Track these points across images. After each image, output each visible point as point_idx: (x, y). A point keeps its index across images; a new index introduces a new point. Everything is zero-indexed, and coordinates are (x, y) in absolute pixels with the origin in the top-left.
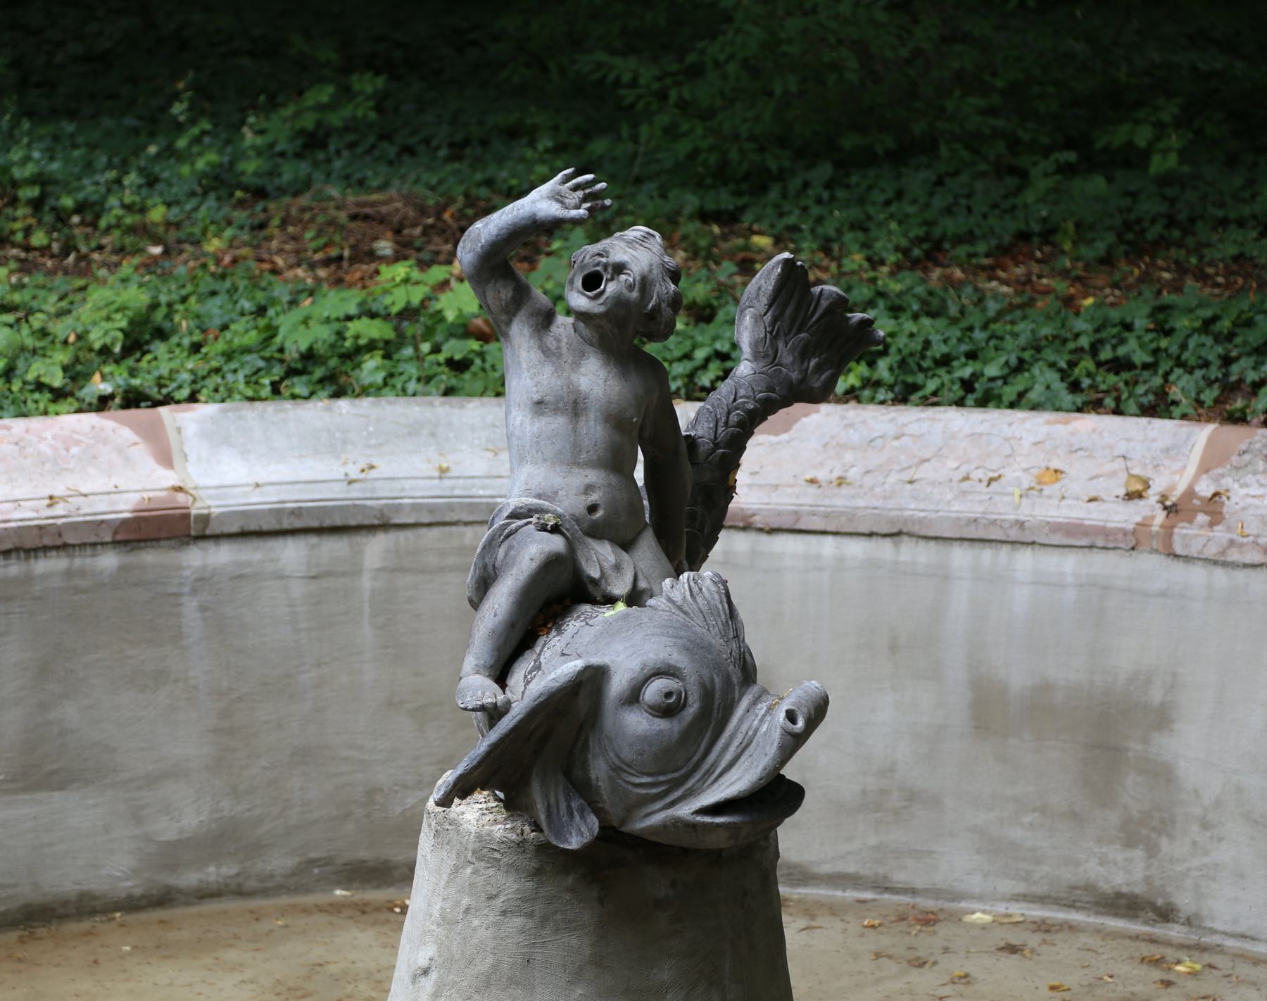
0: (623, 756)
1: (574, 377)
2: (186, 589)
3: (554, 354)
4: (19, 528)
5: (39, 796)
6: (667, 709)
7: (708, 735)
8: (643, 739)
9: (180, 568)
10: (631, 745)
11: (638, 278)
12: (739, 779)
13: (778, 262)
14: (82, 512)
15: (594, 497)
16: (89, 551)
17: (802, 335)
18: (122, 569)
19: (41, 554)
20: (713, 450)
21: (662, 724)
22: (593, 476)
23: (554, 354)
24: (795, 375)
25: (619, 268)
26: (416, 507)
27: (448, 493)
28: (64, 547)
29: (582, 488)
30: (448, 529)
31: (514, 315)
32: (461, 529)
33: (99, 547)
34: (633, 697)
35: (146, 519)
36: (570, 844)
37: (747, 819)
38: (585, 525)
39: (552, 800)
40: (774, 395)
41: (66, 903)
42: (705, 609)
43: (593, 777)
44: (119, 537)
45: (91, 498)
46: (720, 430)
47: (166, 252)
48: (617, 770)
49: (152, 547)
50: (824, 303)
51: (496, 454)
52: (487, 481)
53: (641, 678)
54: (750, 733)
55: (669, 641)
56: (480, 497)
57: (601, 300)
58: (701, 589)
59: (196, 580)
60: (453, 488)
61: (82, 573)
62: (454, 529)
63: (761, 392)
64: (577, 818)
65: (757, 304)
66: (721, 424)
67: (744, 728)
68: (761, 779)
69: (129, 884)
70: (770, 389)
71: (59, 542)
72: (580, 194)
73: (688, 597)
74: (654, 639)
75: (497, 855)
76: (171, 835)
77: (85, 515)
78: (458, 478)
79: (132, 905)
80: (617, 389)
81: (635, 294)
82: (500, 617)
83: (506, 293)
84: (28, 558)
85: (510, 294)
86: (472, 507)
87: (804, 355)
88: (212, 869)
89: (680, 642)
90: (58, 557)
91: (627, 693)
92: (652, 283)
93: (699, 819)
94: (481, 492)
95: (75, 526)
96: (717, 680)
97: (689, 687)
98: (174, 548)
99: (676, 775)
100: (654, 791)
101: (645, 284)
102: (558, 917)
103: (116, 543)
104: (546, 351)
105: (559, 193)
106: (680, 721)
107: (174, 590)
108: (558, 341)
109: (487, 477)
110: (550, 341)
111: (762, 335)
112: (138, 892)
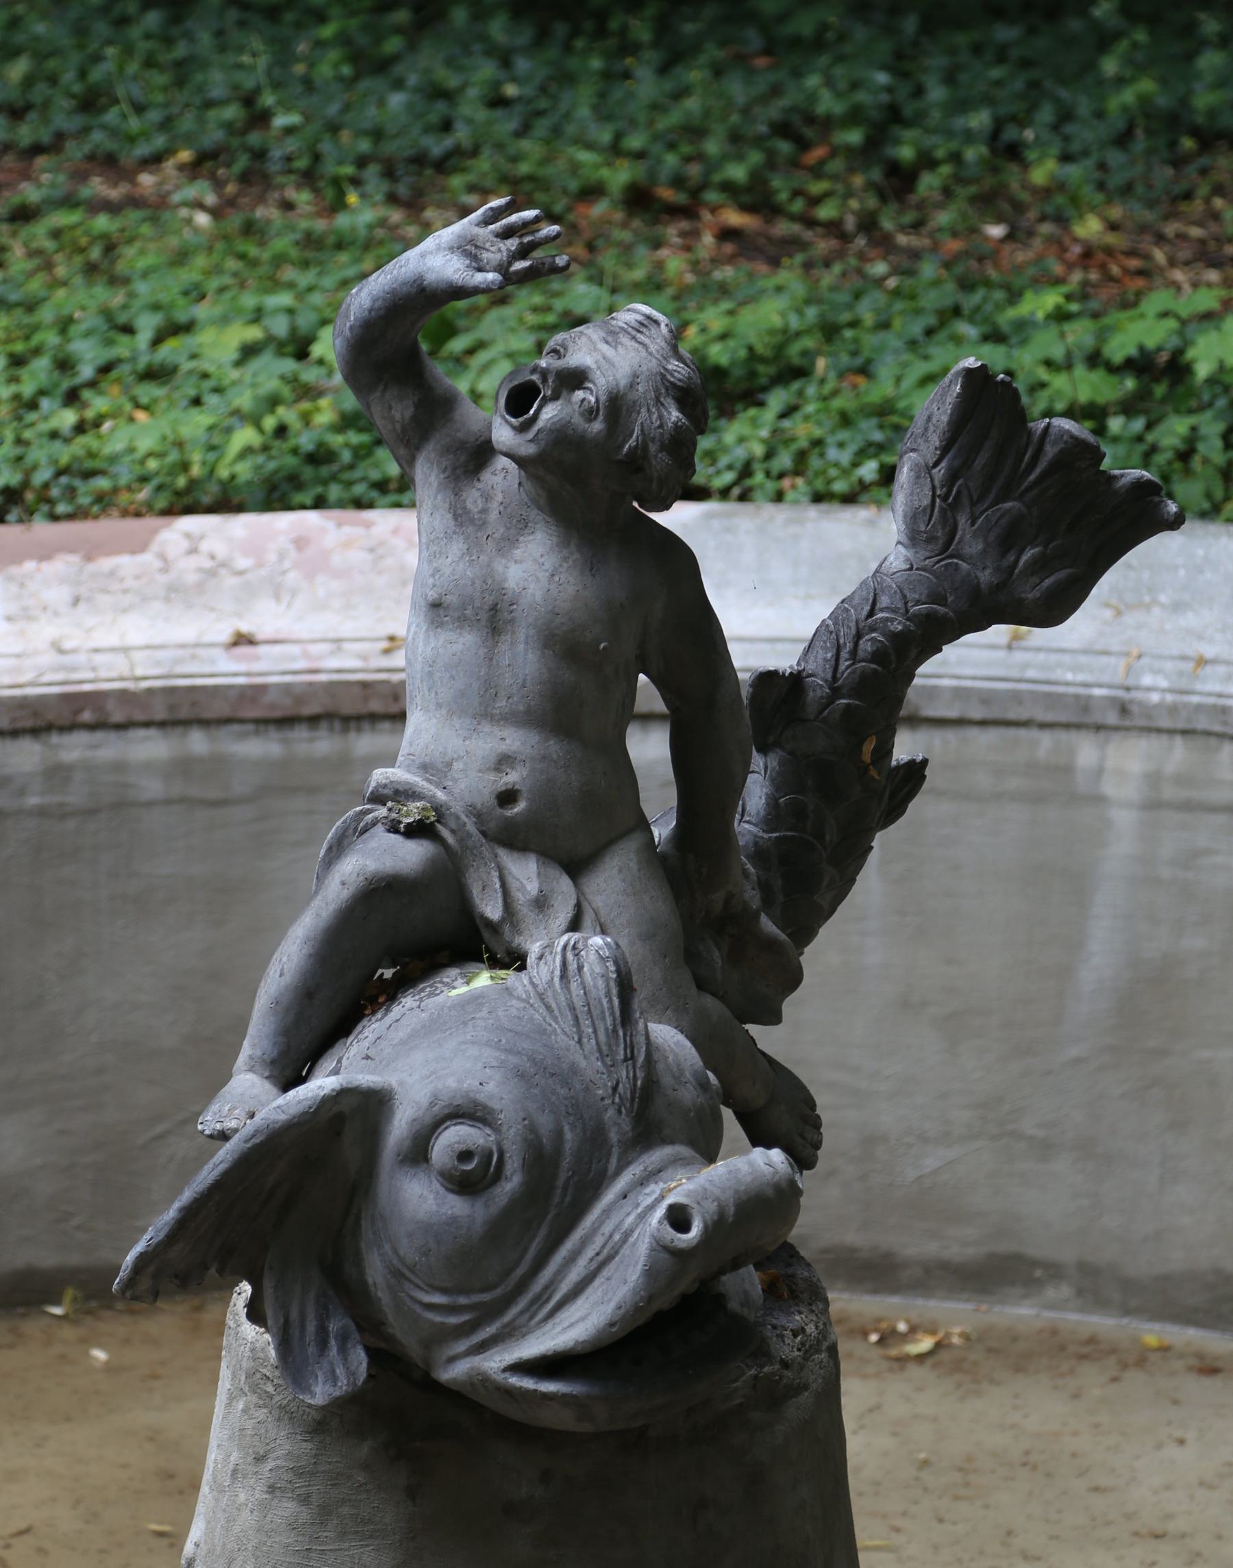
0: (402, 1252)
1: (499, 565)
3: (472, 521)
4: (332, 684)
6: (470, 1178)
7: (543, 1232)
8: (426, 1227)
10: (410, 1235)
11: (603, 398)
12: (583, 1319)
13: (957, 374)
15: (512, 778)
17: (1008, 505)
19: (366, 725)
20: (831, 700)
21: (457, 1206)
22: (514, 740)
23: (472, 521)
25: (575, 379)
26: (960, 694)
27: (1014, 673)
30: (1012, 732)
31: (418, 448)
32: (1034, 733)
34: (417, 1152)
36: (313, 1395)
37: (595, 1390)
39: (294, 1315)
40: (942, 610)
42: (579, 1003)
43: (370, 1280)
47: (1010, 237)
48: (397, 1274)
50: (1050, 451)
51: (1119, 613)
52: (1083, 659)
53: (428, 1120)
54: (617, 1237)
55: (490, 1055)
56: (1067, 684)
57: (531, 435)
58: (580, 968)
60: (1026, 666)
62: (1022, 733)
63: (918, 602)
64: (333, 1351)
65: (923, 447)
66: (844, 654)
67: (607, 1228)
68: (612, 1325)
70: (936, 597)
72: (512, 244)
73: (557, 980)
74: (473, 1051)
75: (270, 1389)
78: (1038, 650)
80: (571, 590)
81: (597, 426)
82: (287, 979)
83: (403, 410)
84: (345, 730)
85: (409, 413)
86: (1051, 700)
87: (1010, 539)
89: (514, 1060)
91: (407, 1143)
92: (634, 407)
93: (515, 1381)
94: (1069, 677)
96: (568, 1136)
97: (507, 1145)
99: (486, 1297)
100: (453, 1320)
101: (616, 407)
102: (345, 1510)
104: (460, 516)
105: (472, 241)
106: (486, 1205)
108: (487, 498)
109: (1086, 652)
110: (472, 498)
111: (926, 502)
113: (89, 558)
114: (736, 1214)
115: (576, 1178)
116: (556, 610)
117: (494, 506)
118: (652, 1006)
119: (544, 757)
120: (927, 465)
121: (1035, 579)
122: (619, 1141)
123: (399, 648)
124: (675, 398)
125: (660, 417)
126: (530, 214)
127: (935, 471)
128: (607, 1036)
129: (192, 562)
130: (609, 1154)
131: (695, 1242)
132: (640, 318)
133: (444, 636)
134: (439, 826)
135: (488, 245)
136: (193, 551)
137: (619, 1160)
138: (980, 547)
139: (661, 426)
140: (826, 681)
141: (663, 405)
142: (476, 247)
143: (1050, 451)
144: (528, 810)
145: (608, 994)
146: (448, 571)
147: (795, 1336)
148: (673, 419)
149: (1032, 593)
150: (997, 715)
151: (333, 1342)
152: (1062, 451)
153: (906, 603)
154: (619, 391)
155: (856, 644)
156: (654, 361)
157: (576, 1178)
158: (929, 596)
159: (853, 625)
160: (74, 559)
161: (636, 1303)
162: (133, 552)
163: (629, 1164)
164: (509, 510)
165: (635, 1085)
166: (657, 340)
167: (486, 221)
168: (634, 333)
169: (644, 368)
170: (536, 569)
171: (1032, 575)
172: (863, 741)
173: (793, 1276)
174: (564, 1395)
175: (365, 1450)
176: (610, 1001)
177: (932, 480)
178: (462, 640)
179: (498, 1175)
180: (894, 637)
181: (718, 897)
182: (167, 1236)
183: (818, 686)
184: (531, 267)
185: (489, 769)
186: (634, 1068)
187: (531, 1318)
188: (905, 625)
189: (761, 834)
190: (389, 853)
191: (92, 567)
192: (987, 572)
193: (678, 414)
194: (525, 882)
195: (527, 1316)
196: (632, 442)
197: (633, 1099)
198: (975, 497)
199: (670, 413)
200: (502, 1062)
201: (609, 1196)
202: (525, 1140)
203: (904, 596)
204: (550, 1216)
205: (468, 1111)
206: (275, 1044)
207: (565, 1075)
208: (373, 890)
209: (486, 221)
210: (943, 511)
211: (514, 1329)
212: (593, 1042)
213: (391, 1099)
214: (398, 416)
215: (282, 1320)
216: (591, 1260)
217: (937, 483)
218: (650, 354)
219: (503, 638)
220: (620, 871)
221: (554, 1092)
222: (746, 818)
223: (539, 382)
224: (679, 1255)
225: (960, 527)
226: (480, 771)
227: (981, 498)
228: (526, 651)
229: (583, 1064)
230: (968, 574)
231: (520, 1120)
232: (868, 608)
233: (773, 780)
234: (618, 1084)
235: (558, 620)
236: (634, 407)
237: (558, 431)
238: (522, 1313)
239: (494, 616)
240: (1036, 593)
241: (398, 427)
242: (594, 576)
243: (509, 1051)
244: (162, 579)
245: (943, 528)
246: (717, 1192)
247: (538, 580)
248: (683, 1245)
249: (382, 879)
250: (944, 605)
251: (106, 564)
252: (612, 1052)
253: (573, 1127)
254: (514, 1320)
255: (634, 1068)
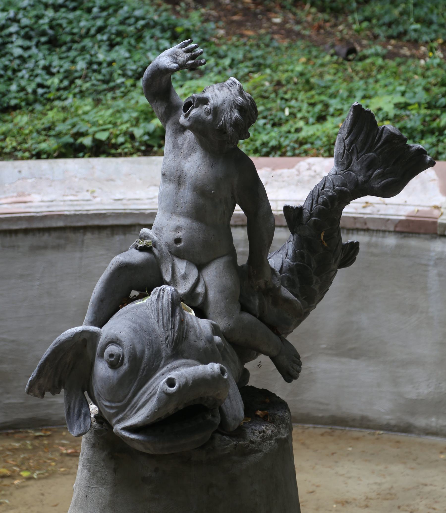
1: (182, 163)
2: (432, 263)
5: (344, 360)
9: (429, 251)
11: (211, 108)
14: (380, 213)
15: (180, 234)
16: (381, 234)
18: (398, 247)
19: (355, 232)
22: (182, 221)
23: (178, 147)
24: (360, 178)
25: (205, 101)
28: (368, 230)
29: (175, 227)
33: (387, 233)
35: (412, 221)
37: (146, 439)
38: (173, 250)
39: (72, 405)
41: (354, 420)
44: (398, 229)
45: (388, 206)
46: (314, 205)
49: (416, 237)
50: (384, 136)
58: (163, 297)
59: (437, 259)
61: (376, 245)
63: (338, 186)
64: (82, 419)
66: (314, 202)
68: (148, 417)
69: (388, 417)
71: (365, 227)
72: (189, 55)
74: (124, 321)
76: (412, 395)
77: (381, 215)
79: (389, 428)
80: (203, 172)
81: (210, 117)
85: (163, 110)
87: (370, 165)
88: (434, 419)
89: (134, 325)
90: (364, 235)
95: (374, 220)
98: (427, 239)
99: (119, 404)
101: (216, 111)
103: (396, 232)
106: (118, 373)
107: (424, 262)
108: (184, 140)
110: (180, 140)
112: (393, 422)
113: (273, 169)
114: (192, 383)
115: (148, 367)
116: (198, 179)
117: (186, 143)
118: (220, 315)
119: (191, 228)
120: (343, 139)
121: (379, 180)
122: (165, 356)
123: (369, 206)
124: (238, 109)
125: (231, 115)
126: (193, 45)
127: (346, 141)
128: (167, 320)
129: (308, 173)
130: (161, 360)
131: (174, 391)
132: (231, 82)
133: (166, 185)
134: (154, 248)
135: (180, 55)
136: (309, 169)
137: (164, 362)
138: (359, 168)
139: (231, 118)
140: (309, 211)
141: (233, 111)
142: (177, 55)
143: (384, 136)
144: (184, 245)
145: (168, 306)
146: (167, 164)
147: (260, 433)
148: (235, 116)
149: (377, 185)
150: (363, 226)
151: (82, 416)
152: (387, 136)
153: (334, 186)
154: (217, 106)
155: (318, 199)
156: (232, 96)
157: (148, 367)
158: (341, 184)
159: (317, 192)
160: (269, 169)
161: (155, 410)
162: (289, 168)
163: (168, 364)
164: (190, 144)
165: (174, 337)
166: (235, 90)
167: (181, 47)
168: (229, 87)
169: (228, 98)
170: (194, 164)
171: (378, 179)
172: (321, 233)
173: (276, 414)
174: (137, 440)
175: (103, 455)
176: (169, 308)
177: (344, 144)
178: (170, 187)
179: (122, 363)
180: (329, 197)
181: (262, 282)
182: (36, 375)
183: (306, 211)
184: (194, 63)
185: (173, 231)
186: (174, 332)
187: (131, 413)
188: (333, 193)
189: (291, 262)
190: (134, 256)
191: (274, 173)
192: (361, 177)
193: (238, 115)
194: (180, 269)
195: (130, 412)
196: (221, 123)
197: (172, 342)
198: (359, 150)
199: (234, 114)
200: (130, 326)
201: (158, 374)
202: (130, 352)
203: (333, 183)
204: (138, 379)
205: (115, 341)
206: (92, 316)
207: (149, 332)
208: (121, 267)
209: (181, 47)
210: (347, 155)
211: (127, 416)
212: (162, 322)
213: (100, 335)
214: (160, 111)
215: (68, 407)
216: (148, 395)
217: (346, 145)
218: (232, 94)
219: (182, 187)
220: (216, 269)
221: (144, 337)
222: (288, 257)
223: (192, 101)
224: (168, 395)
225: (353, 160)
226: (170, 231)
227: (361, 151)
228: (188, 192)
229: (158, 329)
230: (354, 177)
231: (129, 345)
232: (322, 187)
233: (294, 244)
234: (168, 336)
235: (198, 182)
236: (222, 111)
237: (196, 118)
238: (129, 411)
239: (179, 179)
240: (379, 185)
241: (160, 114)
242: (212, 168)
243: (133, 322)
244: (297, 178)
245: (347, 161)
246: (187, 375)
247: (194, 168)
248: (170, 392)
249: (124, 264)
250: (346, 187)
251: (279, 172)
252: (167, 326)
253: (149, 349)
254: (127, 413)
255: (174, 332)
